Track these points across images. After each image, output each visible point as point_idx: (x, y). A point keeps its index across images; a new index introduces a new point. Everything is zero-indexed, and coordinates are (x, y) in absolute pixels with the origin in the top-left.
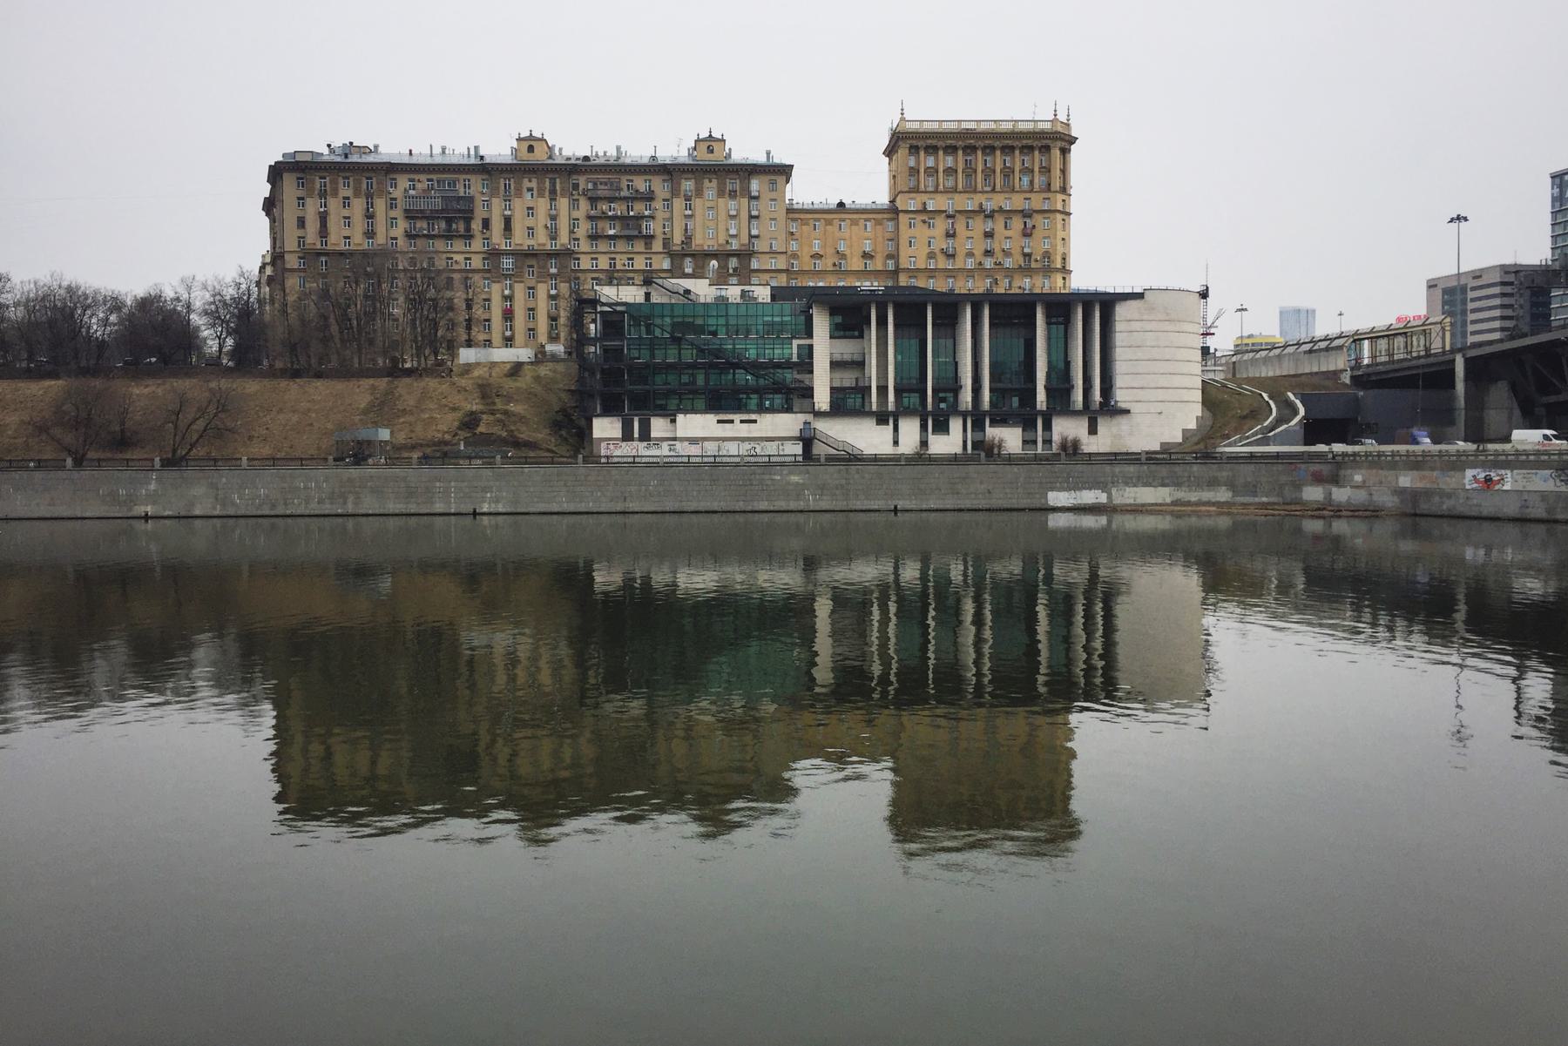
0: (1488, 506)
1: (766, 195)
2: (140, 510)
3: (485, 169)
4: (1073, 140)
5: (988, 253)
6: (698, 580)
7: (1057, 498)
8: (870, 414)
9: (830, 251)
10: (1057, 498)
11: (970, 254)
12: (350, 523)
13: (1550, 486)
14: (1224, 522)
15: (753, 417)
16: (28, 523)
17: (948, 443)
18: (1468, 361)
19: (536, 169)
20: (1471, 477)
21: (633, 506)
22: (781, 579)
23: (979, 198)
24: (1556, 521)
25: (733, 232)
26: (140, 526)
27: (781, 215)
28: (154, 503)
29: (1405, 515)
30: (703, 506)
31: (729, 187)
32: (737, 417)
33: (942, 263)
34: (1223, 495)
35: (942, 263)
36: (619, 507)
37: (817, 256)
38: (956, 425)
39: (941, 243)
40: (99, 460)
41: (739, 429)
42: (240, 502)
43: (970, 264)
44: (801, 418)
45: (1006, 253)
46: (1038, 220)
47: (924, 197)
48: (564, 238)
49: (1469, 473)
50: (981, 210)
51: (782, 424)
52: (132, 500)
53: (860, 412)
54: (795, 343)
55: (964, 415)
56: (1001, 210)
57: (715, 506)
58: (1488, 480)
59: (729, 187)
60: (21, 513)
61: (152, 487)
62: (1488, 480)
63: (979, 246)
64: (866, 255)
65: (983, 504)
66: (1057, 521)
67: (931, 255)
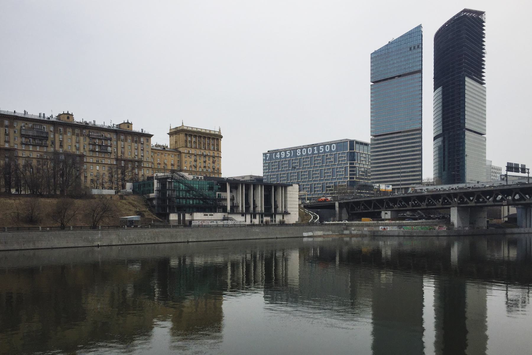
0: (384, 233)
1: (145, 143)
2: (96, 244)
3: (49, 122)
4: (222, 137)
5: (205, 167)
6: (199, 261)
7: (305, 234)
8: (239, 213)
9: (162, 163)
10: (305, 234)
11: (200, 167)
12: (156, 246)
13: (397, 229)
14: (330, 239)
15: (212, 214)
16: (58, 250)
17: (256, 221)
18: (340, 204)
19: (65, 123)
20: (381, 228)
21: (225, 239)
22: (219, 260)
23: (202, 151)
24: (439, 236)
25: (136, 154)
26: (96, 249)
27: (150, 150)
28: (100, 241)
29: (371, 236)
30: (240, 238)
31: (135, 139)
32: (208, 214)
33: (194, 169)
34: (330, 233)
35: (194, 169)
36: (221, 239)
37: (159, 164)
38: (258, 216)
39: (193, 163)
40: (29, 228)
41: (209, 217)
42: (126, 241)
43: (200, 170)
44: (223, 214)
45: (209, 168)
46: (216, 159)
47: (189, 149)
48: (82, 150)
49: (380, 227)
50: (203, 155)
51: (219, 216)
52: (93, 241)
53: (237, 213)
54: (217, 193)
55: (259, 214)
56: (207, 155)
57: (242, 238)
58: (384, 229)
59: (135, 139)
60: (58, 246)
61: (100, 235)
62: (384, 229)
63: (203, 165)
64: (172, 165)
65: (292, 236)
66: (305, 240)
67: (191, 166)
